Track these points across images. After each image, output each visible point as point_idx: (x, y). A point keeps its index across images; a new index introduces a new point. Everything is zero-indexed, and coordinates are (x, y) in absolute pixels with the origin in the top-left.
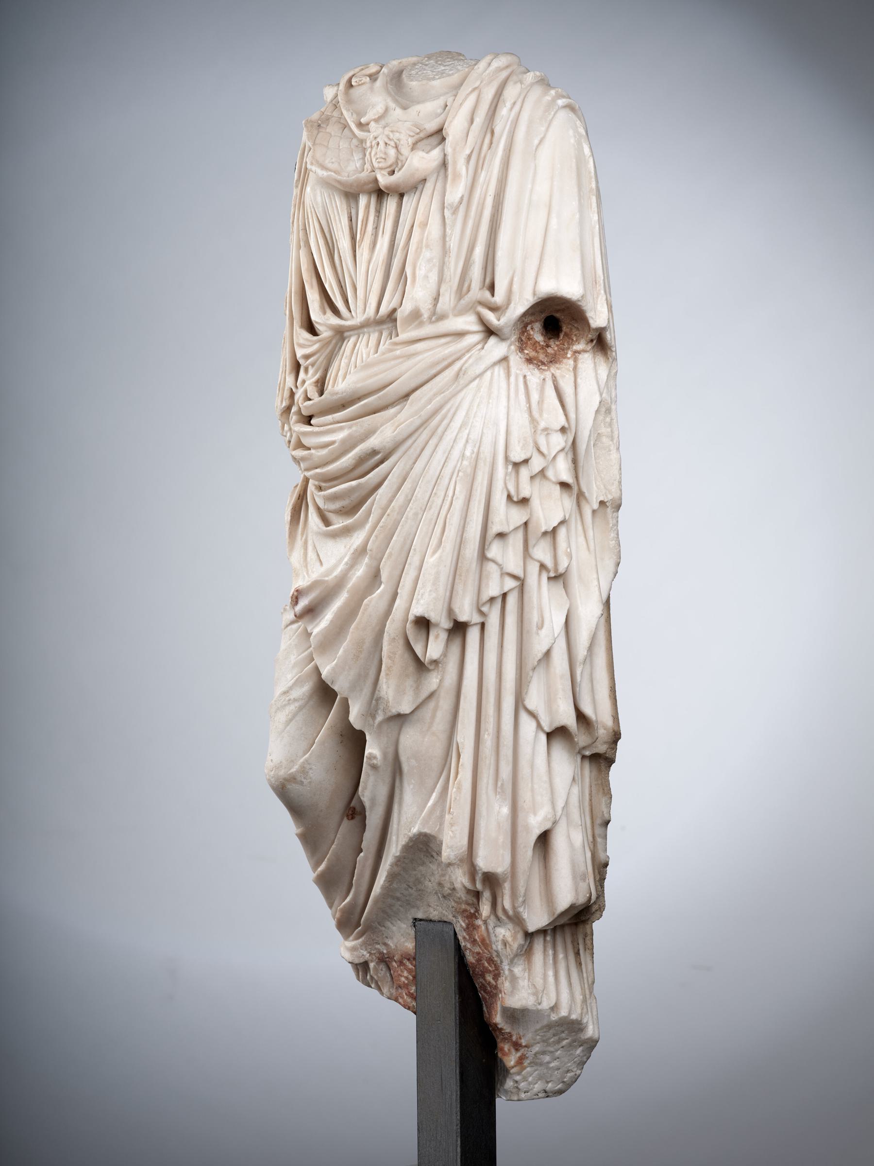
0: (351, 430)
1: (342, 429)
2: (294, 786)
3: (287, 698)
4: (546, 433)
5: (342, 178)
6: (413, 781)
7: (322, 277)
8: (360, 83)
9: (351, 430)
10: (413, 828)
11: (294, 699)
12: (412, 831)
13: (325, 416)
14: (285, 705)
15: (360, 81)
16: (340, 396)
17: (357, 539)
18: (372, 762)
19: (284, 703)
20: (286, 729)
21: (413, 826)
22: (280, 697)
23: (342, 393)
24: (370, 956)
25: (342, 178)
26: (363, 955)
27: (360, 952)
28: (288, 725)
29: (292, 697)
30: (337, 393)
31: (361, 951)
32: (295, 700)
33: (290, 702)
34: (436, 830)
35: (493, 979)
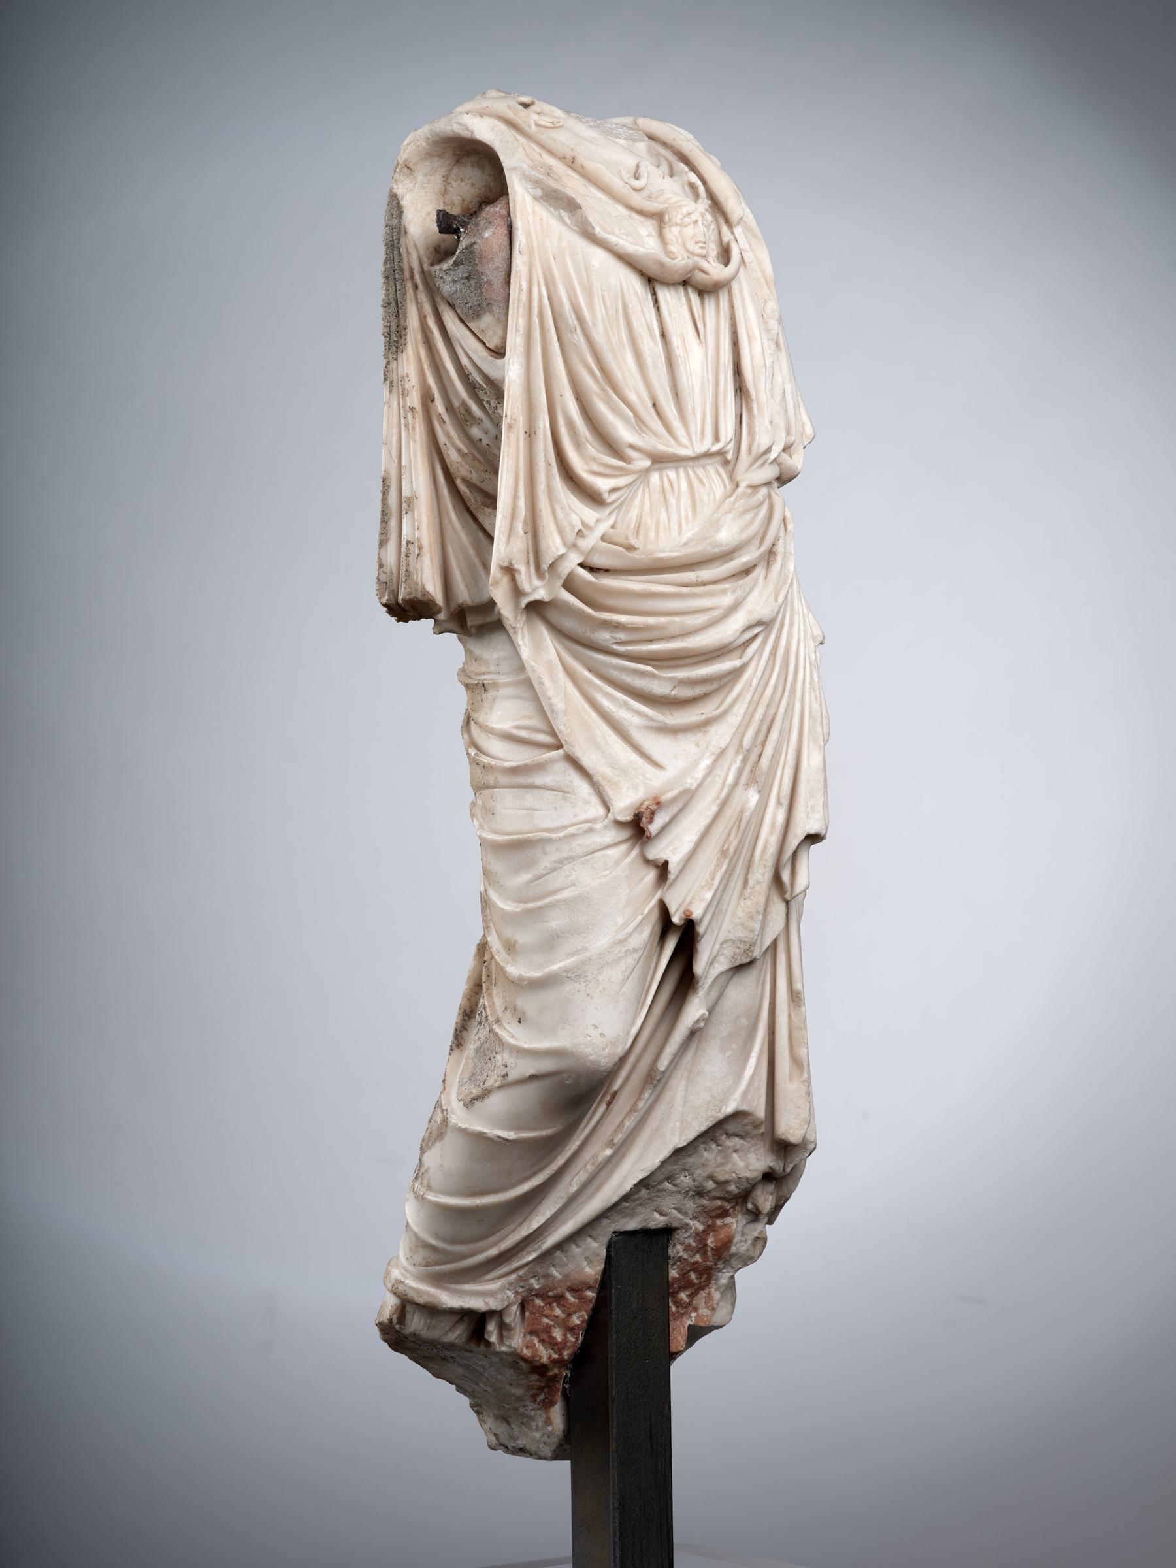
0: (736, 595)
1: (724, 592)
2: (792, 574)
3: (624, 949)
4: (756, 1124)
5: (577, 326)
6: (733, 1046)
7: (622, 404)
8: (557, 125)
9: (736, 595)
10: (724, 1107)
11: (633, 949)
12: (722, 1111)
13: (630, 698)
14: (620, 958)
15: (558, 122)
16: (723, 548)
17: (721, 734)
18: (699, 1026)
19: (619, 955)
20: (622, 991)
21: (725, 1105)
22: (613, 947)
23: (726, 546)
24: (514, 1297)
25: (577, 326)
26: (508, 1297)
27: (505, 1294)
28: (623, 986)
29: (631, 947)
30: (720, 546)
31: (508, 1292)
32: (635, 950)
33: (628, 953)
34: (754, 1105)
35: (688, 1296)
